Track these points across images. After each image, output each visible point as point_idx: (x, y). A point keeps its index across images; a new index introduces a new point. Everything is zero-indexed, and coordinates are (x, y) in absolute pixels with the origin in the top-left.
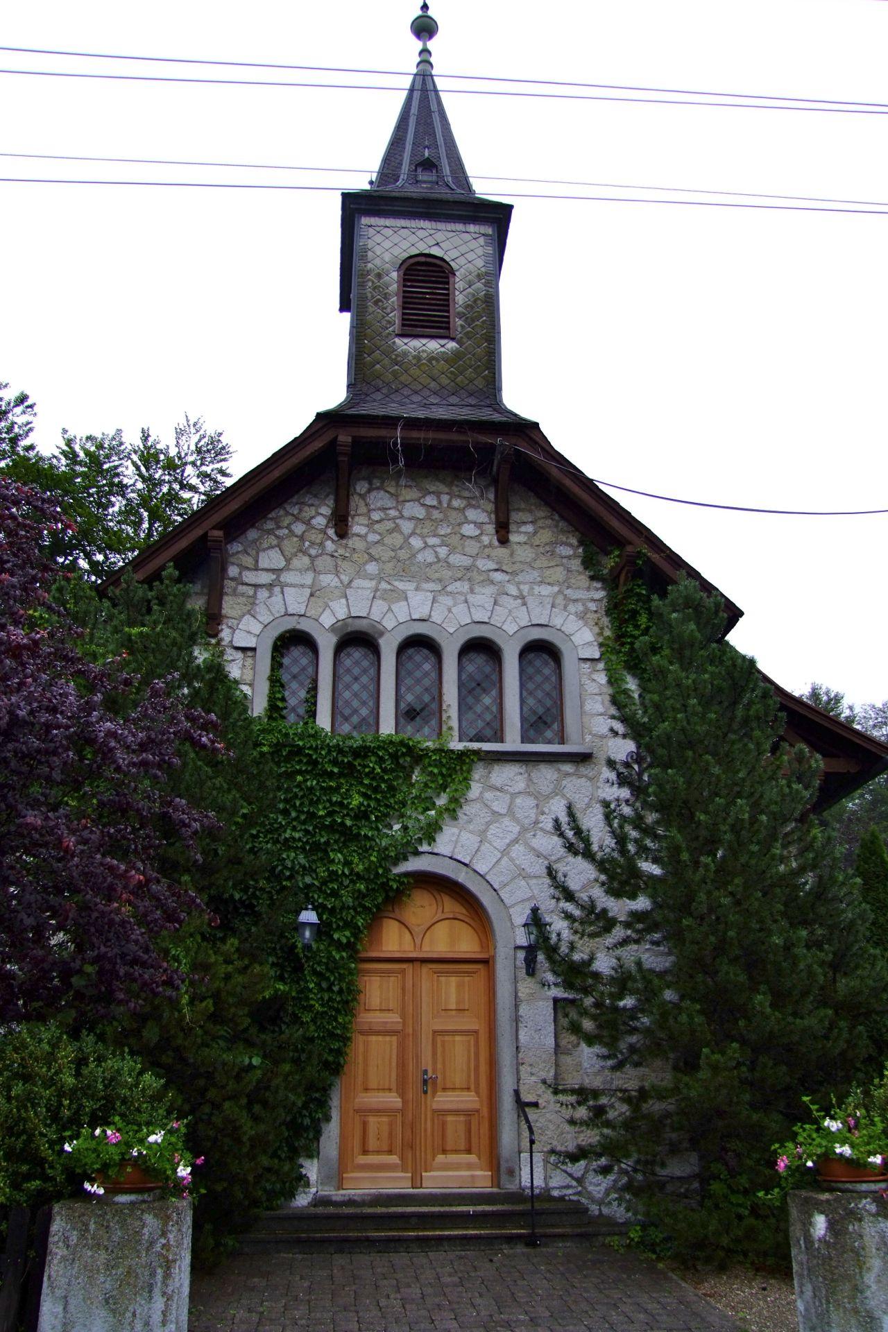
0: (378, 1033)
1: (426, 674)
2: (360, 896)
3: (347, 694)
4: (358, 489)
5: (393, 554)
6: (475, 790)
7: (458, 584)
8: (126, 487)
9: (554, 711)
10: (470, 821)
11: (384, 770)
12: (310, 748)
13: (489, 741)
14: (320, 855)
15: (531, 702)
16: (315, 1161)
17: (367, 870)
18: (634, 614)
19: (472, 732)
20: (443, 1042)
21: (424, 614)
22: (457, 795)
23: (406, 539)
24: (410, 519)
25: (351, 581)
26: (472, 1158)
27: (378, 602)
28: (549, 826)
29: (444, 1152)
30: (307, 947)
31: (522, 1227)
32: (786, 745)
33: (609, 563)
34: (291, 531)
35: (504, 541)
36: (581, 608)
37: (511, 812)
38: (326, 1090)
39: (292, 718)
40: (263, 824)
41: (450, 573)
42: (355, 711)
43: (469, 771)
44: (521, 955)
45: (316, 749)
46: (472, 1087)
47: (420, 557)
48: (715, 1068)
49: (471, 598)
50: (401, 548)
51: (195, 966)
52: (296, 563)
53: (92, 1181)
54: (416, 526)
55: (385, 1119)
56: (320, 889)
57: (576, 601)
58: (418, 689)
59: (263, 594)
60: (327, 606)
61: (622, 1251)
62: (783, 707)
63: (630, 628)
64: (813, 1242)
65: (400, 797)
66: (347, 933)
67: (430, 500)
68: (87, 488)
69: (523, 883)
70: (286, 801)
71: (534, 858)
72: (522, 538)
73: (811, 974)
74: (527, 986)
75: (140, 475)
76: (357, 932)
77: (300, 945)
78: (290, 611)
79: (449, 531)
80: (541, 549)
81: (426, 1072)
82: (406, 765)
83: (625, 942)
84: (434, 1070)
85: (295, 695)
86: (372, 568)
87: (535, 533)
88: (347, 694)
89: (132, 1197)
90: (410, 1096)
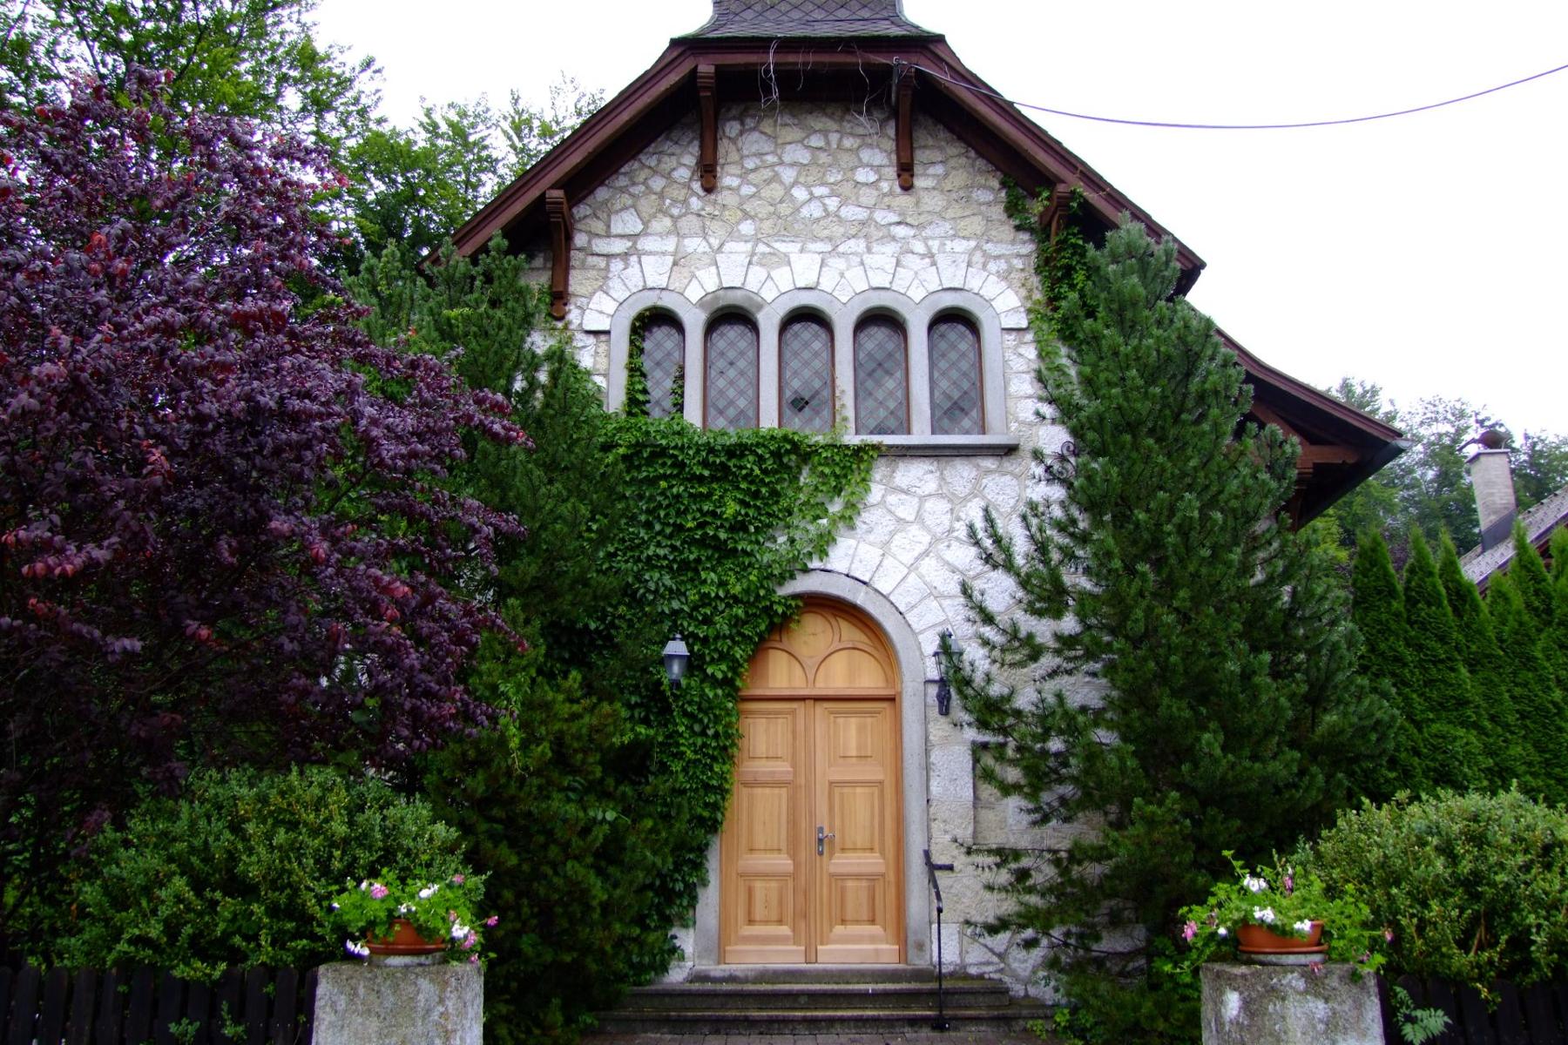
0: (764, 784)
1: (816, 354)
2: (737, 622)
3: (721, 383)
4: (727, 130)
5: (772, 209)
6: (876, 492)
7: (852, 242)
8: (497, 161)
9: (973, 394)
10: (870, 531)
11: (765, 472)
12: (675, 447)
13: (893, 433)
14: (690, 574)
15: (944, 384)
16: (691, 931)
17: (747, 591)
18: (1069, 271)
19: (872, 424)
20: (842, 794)
21: (811, 282)
22: (854, 499)
23: (788, 190)
24: (793, 165)
25: (722, 245)
26: (876, 929)
27: (755, 269)
28: (962, 532)
29: (843, 922)
30: (675, 684)
31: (930, 1009)
32: (1253, 427)
33: (1037, 207)
34: (648, 187)
35: (907, 187)
36: (1003, 265)
37: (919, 518)
38: (702, 849)
39: (656, 413)
40: (623, 540)
41: (842, 230)
42: (731, 403)
43: (868, 471)
44: (933, 690)
45: (682, 449)
46: (877, 846)
47: (805, 212)
48: (1151, 822)
49: (868, 259)
50: (781, 202)
51: (528, 705)
53: (355, 940)
54: (799, 174)
55: (774, 885)
56: (690, 616)
57: (998, 257)
58: (807, 373)
59: (616, 266)
60: (693, 276)
61: (1044, 1036)
62: (1250, 378)
63: (1065, 288)
64: (1223, 1024)
65: (784, 503)
66: (724, 667)
67: (817, 141)
68: (450, 165)
69: (935, 604)
70: (649, 512)
71: (949, 574)
72: (930, 183)
73: (1277, 709)
74: (939, 728)
75: (513, 147)
76: (735, 666)
77: (666, 681)
78: (650, 284)
79: (840, 177)
80: (954, 195)
81: (821, 830)
82: (792, 464)
83: (1053, 674)
84: (832, 828)
85: (659, 387)
86: (747, 228)
87: (946, 175)
88: (721, 383)
89: (407, 960)
90: (803, 855)
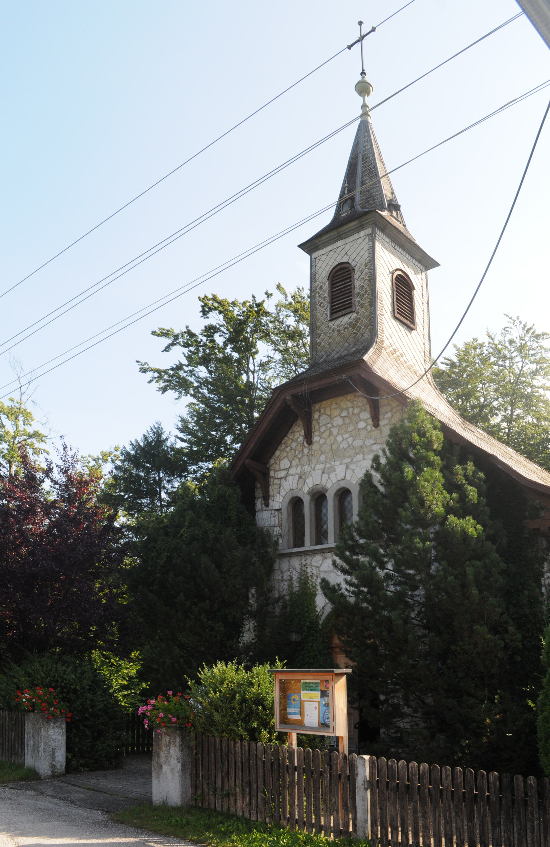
52: (294, 463)
